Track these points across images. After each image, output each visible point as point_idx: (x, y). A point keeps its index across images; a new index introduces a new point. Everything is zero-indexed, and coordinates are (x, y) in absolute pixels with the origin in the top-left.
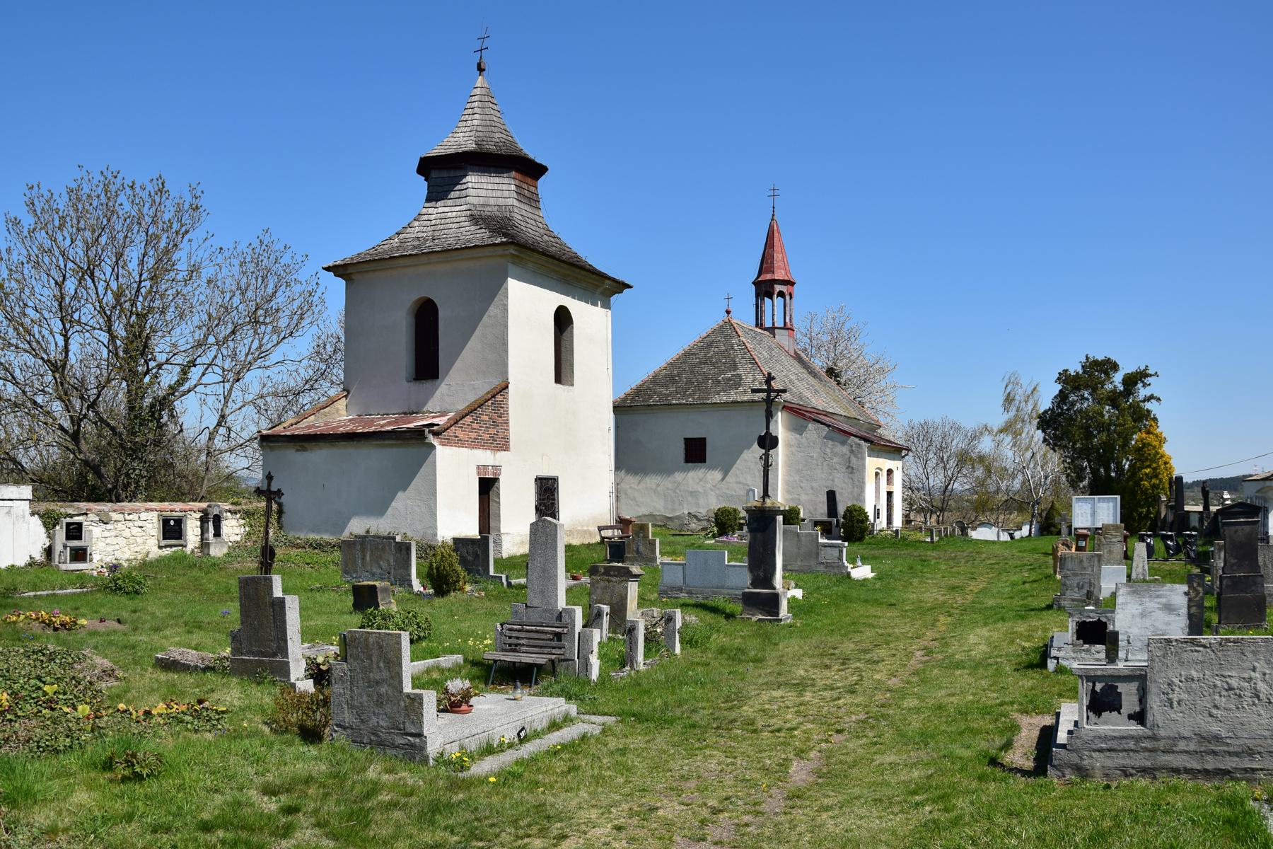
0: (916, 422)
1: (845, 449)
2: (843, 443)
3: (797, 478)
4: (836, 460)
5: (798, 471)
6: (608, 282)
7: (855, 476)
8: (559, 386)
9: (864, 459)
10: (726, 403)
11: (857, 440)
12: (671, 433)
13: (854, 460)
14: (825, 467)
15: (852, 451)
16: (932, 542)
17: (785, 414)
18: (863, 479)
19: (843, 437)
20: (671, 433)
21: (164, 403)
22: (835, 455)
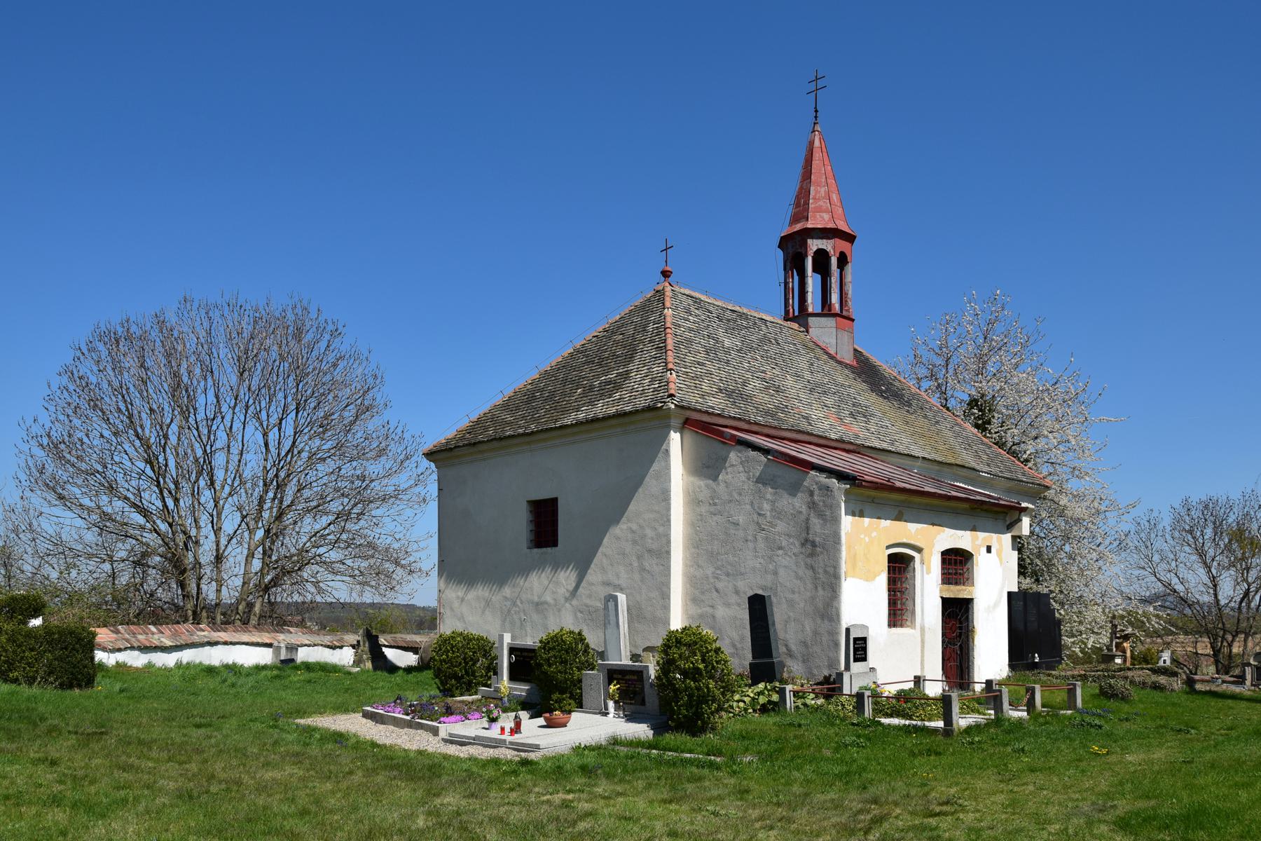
0: (1194, 500)
1: (798, 503)
2: (793, 489)
3: (709, 571)
4: (781, 527)
5: (712, 556)
6: (919, 463)
7: (820, 561)
8: (894, 630)
9: (836, 521)
10: (579, 424)
11: (822, 478)
12: (511, 485)
13: (815, 522)
14: (761, 544)
15: (812, 505)
16: (948, 731)
17: (688, 435)
18: (836, 567)
19: (791, 473)
20: (511, 485)
21: (504, 621)
22: (779, 514)
